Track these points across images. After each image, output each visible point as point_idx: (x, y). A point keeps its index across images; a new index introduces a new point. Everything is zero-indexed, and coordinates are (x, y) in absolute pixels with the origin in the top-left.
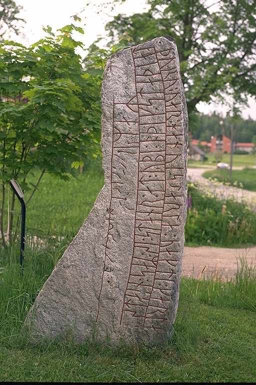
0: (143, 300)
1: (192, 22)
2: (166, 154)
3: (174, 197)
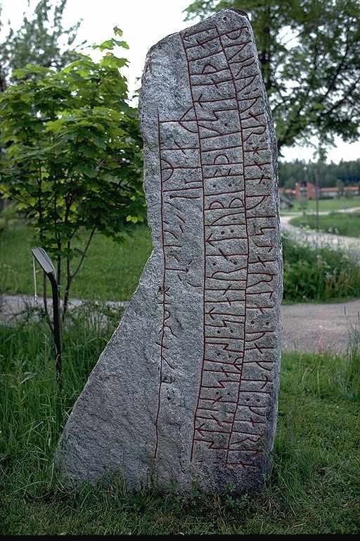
0: (223, 424)
1: (270, 61)
2: (246, 196)
3: (262, 262)
